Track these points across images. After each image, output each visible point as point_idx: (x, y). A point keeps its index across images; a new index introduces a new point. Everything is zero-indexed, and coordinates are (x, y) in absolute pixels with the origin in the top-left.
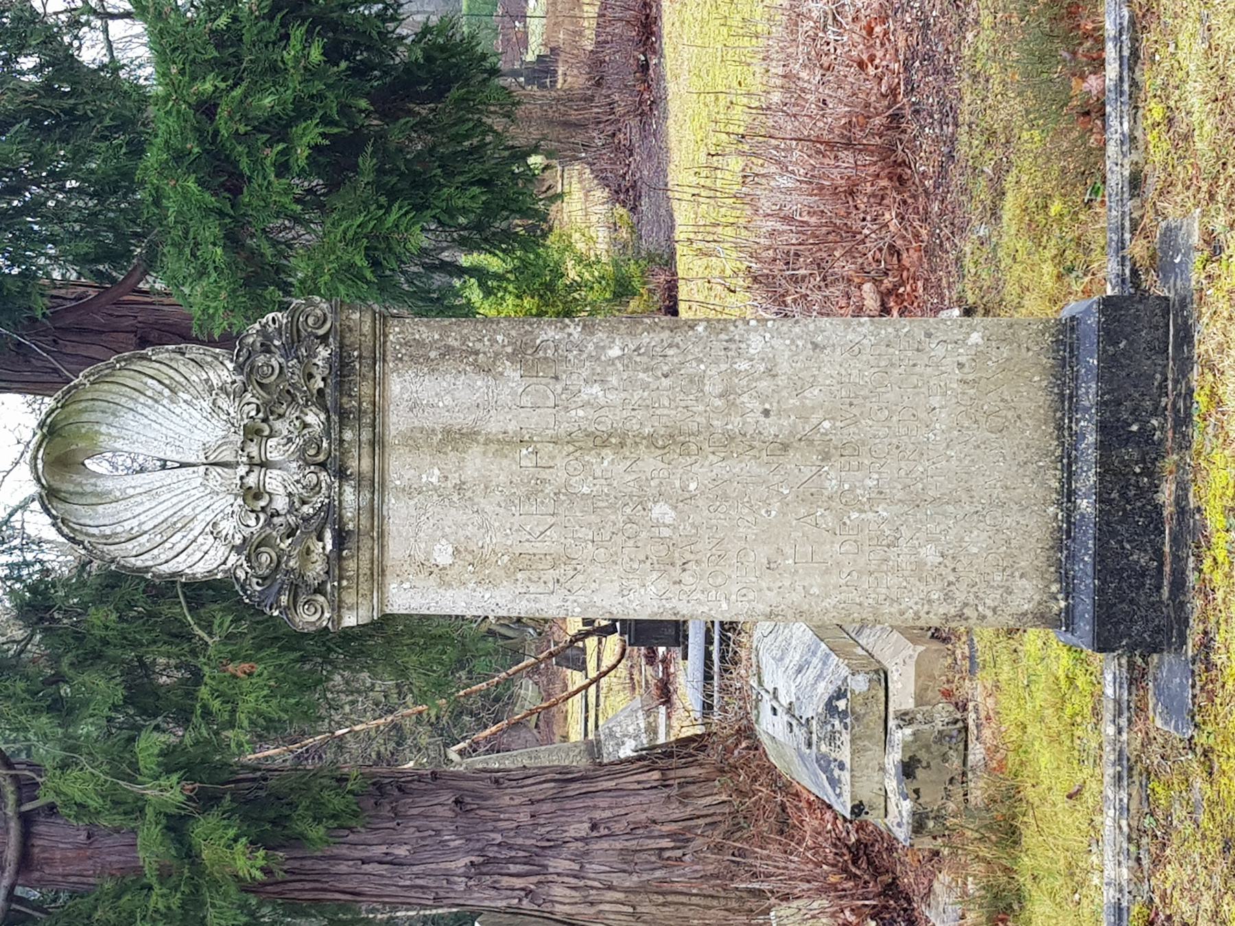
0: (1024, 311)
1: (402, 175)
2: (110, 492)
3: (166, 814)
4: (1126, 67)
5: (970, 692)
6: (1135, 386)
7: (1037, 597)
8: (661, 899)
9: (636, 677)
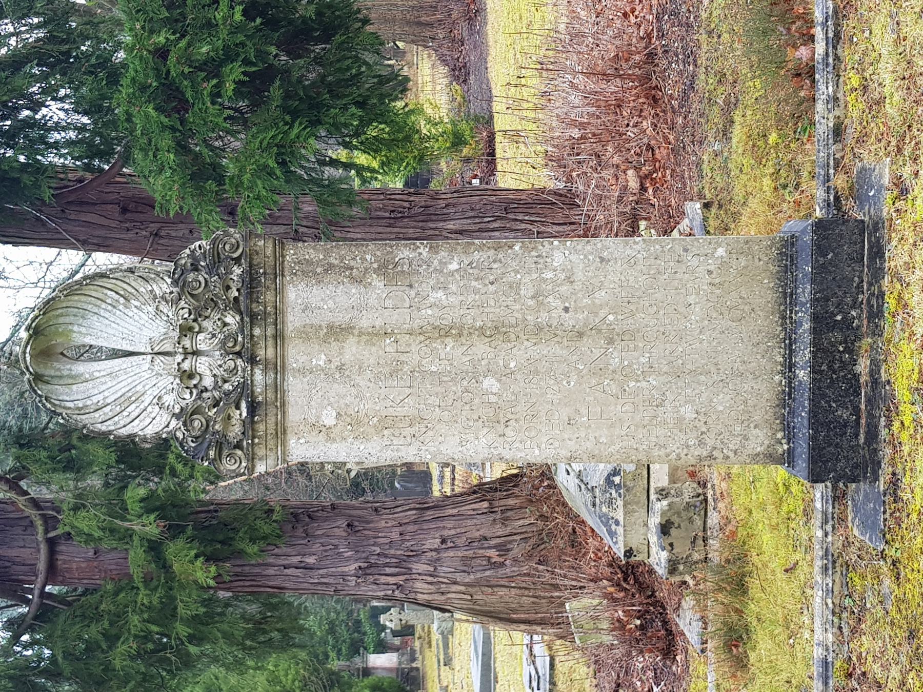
1: (301, 99)
2: (82, 375)
3: (147, 540)
5: (709, 476)
6: (839, 287)
7: (767, 442)
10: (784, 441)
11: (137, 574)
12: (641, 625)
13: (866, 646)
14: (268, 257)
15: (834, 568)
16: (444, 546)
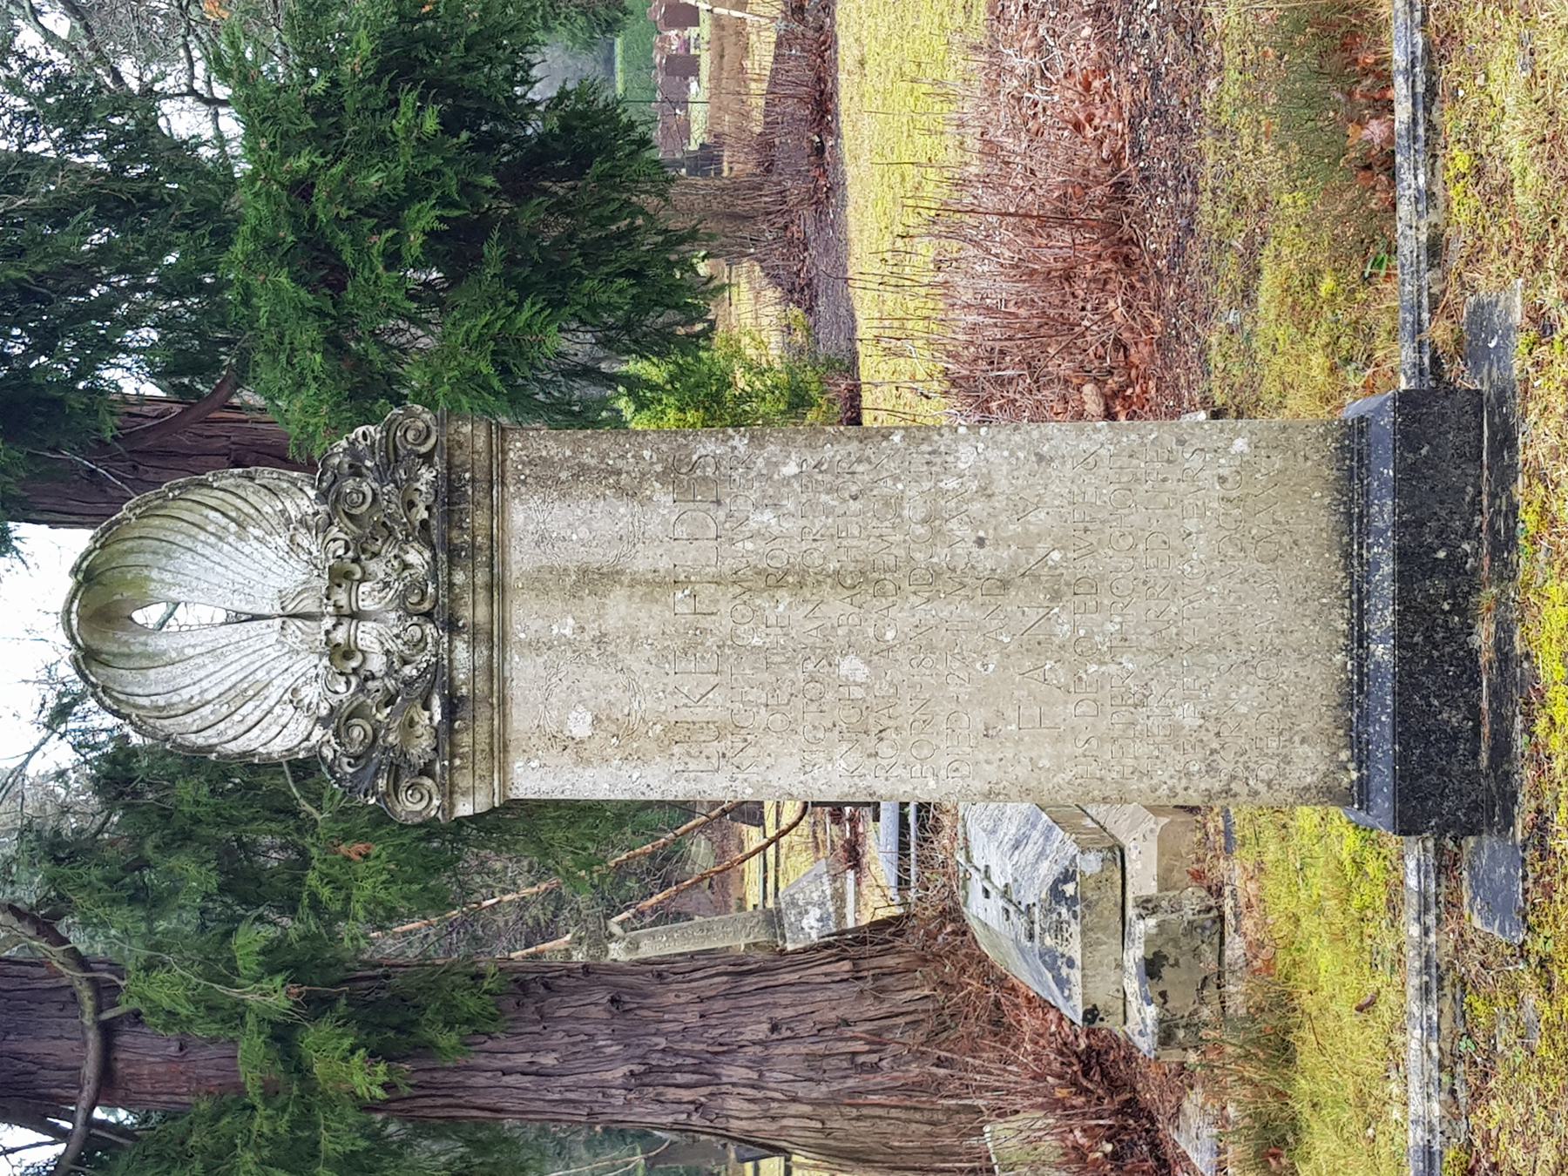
0: (1287, 412)
2: (164, 653)
3: (270, 1022)
4: (1420, 107)
6: (1442, 502)
7: (1322, 767)
8: (854, 1112)
9: (820, 836)
10: (1351, 766)
11: (251, 1079)
12: (1114, 1152)
13: (1497, 1118)
14: (479, 454)
15: (1440, 988)
16: (775, 1036)
